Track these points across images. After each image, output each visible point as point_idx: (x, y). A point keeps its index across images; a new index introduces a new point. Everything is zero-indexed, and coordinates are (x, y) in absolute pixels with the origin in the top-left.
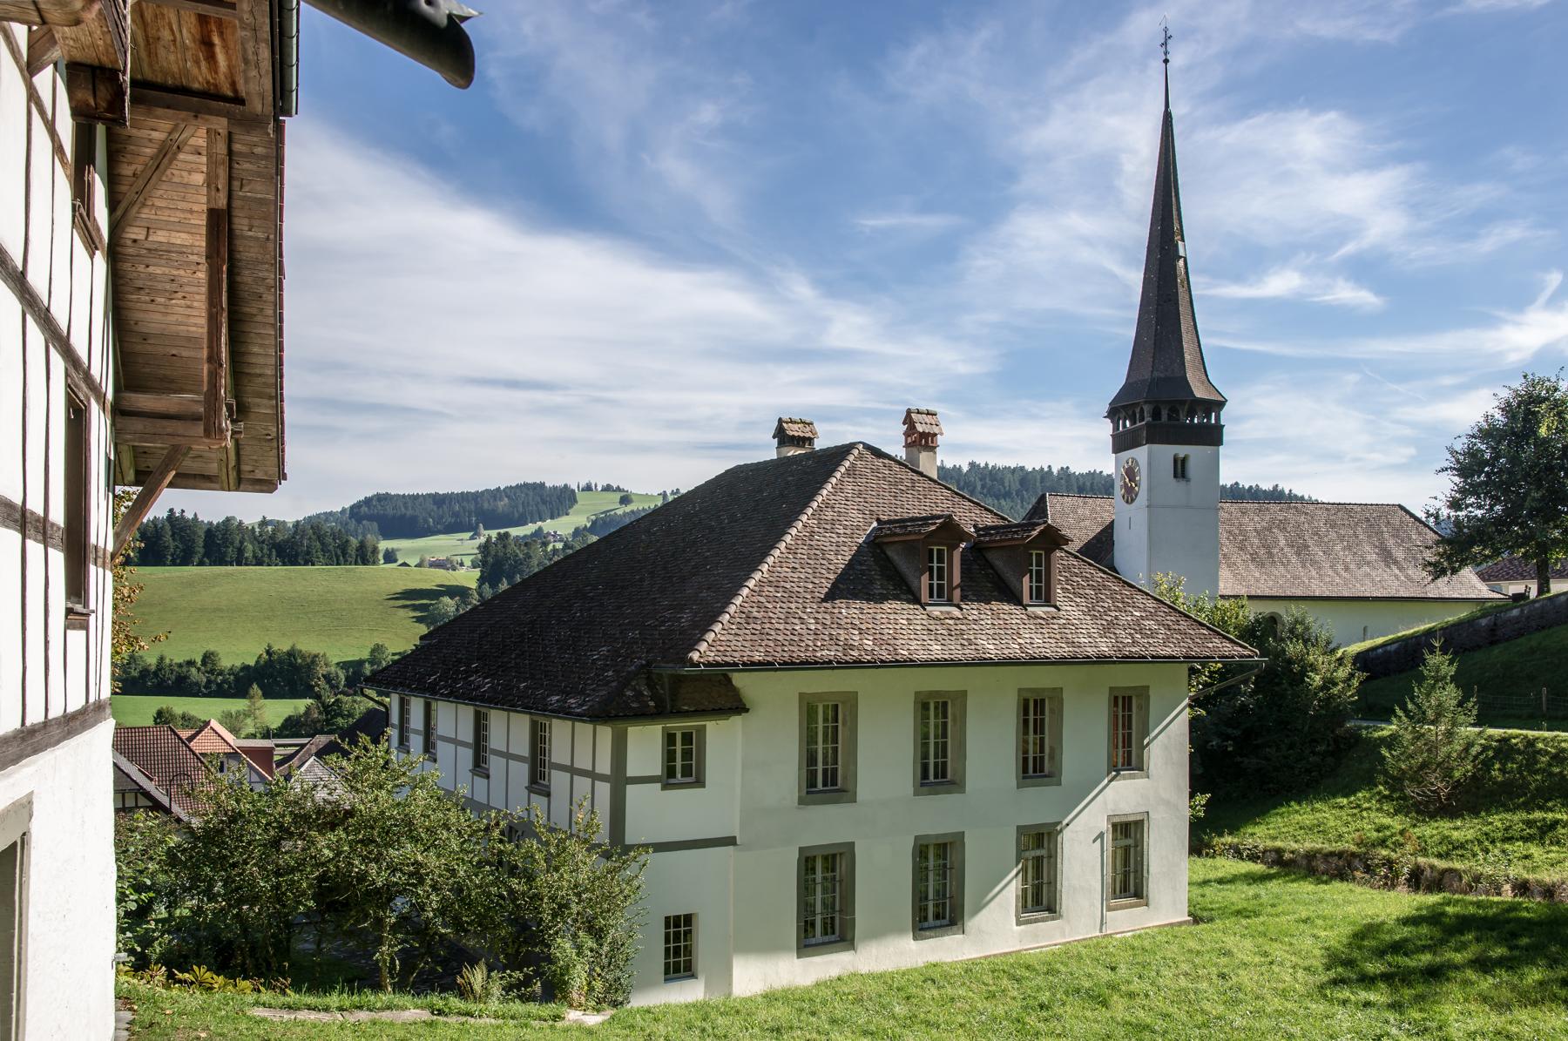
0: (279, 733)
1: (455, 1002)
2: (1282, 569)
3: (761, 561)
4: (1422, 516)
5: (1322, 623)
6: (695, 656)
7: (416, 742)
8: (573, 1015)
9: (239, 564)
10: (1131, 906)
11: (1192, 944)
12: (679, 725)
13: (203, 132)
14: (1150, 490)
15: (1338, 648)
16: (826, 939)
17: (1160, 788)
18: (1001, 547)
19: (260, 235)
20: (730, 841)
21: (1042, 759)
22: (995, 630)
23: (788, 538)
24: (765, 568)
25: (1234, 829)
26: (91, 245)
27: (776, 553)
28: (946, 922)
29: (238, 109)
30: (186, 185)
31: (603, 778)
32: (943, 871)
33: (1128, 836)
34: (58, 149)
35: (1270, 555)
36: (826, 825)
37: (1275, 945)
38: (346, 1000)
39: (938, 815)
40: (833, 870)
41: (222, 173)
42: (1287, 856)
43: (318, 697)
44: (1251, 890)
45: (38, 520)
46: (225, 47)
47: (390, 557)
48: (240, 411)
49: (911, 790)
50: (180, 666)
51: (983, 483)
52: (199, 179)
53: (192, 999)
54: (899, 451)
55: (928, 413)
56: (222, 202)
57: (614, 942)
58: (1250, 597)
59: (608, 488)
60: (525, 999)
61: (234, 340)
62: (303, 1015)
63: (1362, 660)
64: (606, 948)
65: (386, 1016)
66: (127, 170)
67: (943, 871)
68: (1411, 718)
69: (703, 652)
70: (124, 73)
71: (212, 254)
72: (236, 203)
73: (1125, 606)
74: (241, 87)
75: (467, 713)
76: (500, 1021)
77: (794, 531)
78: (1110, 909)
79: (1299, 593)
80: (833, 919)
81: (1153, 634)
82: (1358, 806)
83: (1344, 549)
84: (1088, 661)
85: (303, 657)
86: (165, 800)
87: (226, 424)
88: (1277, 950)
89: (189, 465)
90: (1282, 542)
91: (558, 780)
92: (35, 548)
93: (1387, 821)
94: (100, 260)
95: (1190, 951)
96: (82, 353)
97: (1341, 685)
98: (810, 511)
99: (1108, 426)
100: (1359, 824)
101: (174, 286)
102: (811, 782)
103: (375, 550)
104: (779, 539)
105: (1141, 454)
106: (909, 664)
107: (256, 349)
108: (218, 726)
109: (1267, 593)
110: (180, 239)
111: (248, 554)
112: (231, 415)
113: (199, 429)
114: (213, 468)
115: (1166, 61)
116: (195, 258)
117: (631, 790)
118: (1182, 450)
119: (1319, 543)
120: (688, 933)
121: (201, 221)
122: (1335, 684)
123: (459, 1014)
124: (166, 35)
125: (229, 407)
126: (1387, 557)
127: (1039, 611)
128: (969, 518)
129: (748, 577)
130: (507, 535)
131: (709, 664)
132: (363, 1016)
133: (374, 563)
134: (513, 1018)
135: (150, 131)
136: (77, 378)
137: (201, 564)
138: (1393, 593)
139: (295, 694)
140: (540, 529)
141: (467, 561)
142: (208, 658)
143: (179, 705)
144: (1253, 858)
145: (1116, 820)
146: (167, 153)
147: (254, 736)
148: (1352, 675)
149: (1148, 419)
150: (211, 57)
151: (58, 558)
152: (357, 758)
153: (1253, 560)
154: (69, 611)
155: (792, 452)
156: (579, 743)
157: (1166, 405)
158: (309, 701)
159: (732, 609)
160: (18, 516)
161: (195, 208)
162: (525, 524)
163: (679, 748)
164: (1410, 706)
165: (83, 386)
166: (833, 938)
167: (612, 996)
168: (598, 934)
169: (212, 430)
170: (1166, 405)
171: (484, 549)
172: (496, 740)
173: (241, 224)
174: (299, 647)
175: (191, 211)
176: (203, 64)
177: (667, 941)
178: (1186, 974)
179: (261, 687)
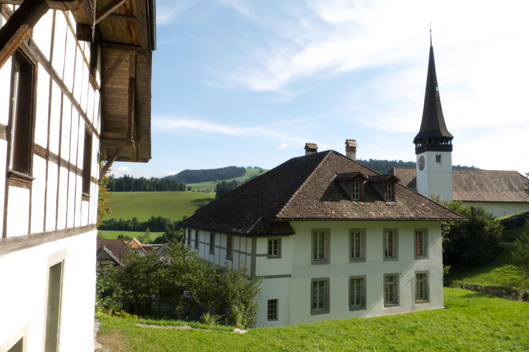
0: (155, 242)
1: (199, 324)
2: (474, 192)
3: (300, 186)
4: (525, 176)
5: (488, 210)
6: (278, 216)
7: (193, 244)
8: (237, 330)
9: (144, 191)
10: (423, 302)
11: (444, 315)
12: (273, 238)
13: (128, 55)
14: (428, 166)
15: (495, 218)
16: (320, 309)
17: (434, 262)
18: (379, 182)
19: (145, 85)
20: (289, 276)
21: (392, 252)
22: (377, 210)
23: (308, 179)
24: (301, 188)
25: (460, 279)
26: (95, 87)
27: (304, 184)
28: (360, 305)
29: (138, 48)
30: (123, 71)
31: (249, 254)
32: (359, 288)
33: (422, 277)
34: (85, 59)
35: (470, 187)
36: (320, 272)
37: (475, 317)
38: (166, 322)
39: (357, 269)
40: (323, 286)
41: (134, 67)
42: (479, 288)
43: (166, 232)
44: (466, 299)
45: (74, 166)
46: (135, 30)
47: (189, 189)
48: (138, 138)
49: (348, 261)
50: (126, 222)
51: (374, 164)
52: (127, 69)
53: (119, 320)
54: (344, 154)
55: (353, 141)
56: (133, 76)
57: (251, 307)
58: (464, 201)
59: (256, 168)
60: (222, 324)
61: (136, 117)
62: (151, 326)
63: (504, 222)
64: (248, 309)
65: (177, 328)
66: (107, 67)
67: (359, 288)
68: (521, 242)
69: (280, 215)
70: (92, 26)
71: (130, 91)
72: (138, 76)
73: (419, 202)
74: (139, 42)
75: (208, 235)
76: (213, 331)
77: (310, 177)
78: (416, 303)
79: (481, 200)
80: (323, 303)
81: (429, 211)
82: (504, 272)
83: (496, 185)
84: (406, 220)
85: (162, 219)
86: (118, 262)
87: (133, 141)
88: (475, 319)
89: (121, 154)
90: (474, 183)
91: (235, 255)
92: (72, 174)
93: (514, 277)
94: (97, 94)
95: (443, 317)
96: (91, 120)
97: (496, 231)
98: (315, 171)
99: (414, 146)
100: (504, 278)
101: (119, 101)
102: (315, 256)
103: (185, 187)
104: (305, 180)
105: (425, 154)
106: (347, 219)
107: (143, 119)
108: (135, 240)
109: (470, 200)
110: (121, 87)
111: (147, 188)
112: (135, 139)
113: (125, 143)
114: (130, 155)
115: (431, 31)
116: (126, 92)
117: (258, 258)
118: (439, 153)
119: (488, 183)
120: (275, 306)
121: (127, 81)
122: (494, 230)
123: (200, 328)
124: (118, 27)
125: (134, 136)
126: (511, 188)
127: (390, 203)
128: (367, 174)
129: (295, 191)
130: (224, 182)
131: (282, 218)
132: (170, 327)
133: (185, 191)
134: (217, 330)
135: (114, 55)
136: (89, 126)
137: (133, 191)
138: (514, 200)
139: (159, 231)
140: (235, 180)
141: (213, 190)
142: (135, 220)
143: (125, 234)
144: (467, 288)
145: (418, 273)
146: (119, 61)
147: (147, 243)
148: (500, 227)
149: (427, 143)
150: (131, 33)
151: (80, 179)
152: (173, 246)
153: (464, 189)
154: (83, 195)
155: (311, 153)
156: (241, 244)
157: (433, 137)
158: (164, 233)
159: (290, 201)
160: (67, 164)
161: (126, 78)
162: (230, 179)
163: (273, 245)
164: (521, 237)
165: (91, 129)
166: (322, 309)
167: (249, 325)
168: (246, 303)
169: (129, 143)
170: (433, 137)
171: (218, 186)
172: (217, 243)
173: (139, 82)
174: (161, 216)
175: (125, 79)
176: (129, 35)
177: (269, 308)
178: (442, 325)
179: (150, 228)
